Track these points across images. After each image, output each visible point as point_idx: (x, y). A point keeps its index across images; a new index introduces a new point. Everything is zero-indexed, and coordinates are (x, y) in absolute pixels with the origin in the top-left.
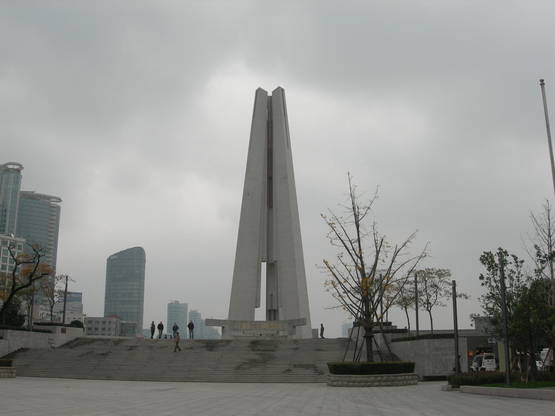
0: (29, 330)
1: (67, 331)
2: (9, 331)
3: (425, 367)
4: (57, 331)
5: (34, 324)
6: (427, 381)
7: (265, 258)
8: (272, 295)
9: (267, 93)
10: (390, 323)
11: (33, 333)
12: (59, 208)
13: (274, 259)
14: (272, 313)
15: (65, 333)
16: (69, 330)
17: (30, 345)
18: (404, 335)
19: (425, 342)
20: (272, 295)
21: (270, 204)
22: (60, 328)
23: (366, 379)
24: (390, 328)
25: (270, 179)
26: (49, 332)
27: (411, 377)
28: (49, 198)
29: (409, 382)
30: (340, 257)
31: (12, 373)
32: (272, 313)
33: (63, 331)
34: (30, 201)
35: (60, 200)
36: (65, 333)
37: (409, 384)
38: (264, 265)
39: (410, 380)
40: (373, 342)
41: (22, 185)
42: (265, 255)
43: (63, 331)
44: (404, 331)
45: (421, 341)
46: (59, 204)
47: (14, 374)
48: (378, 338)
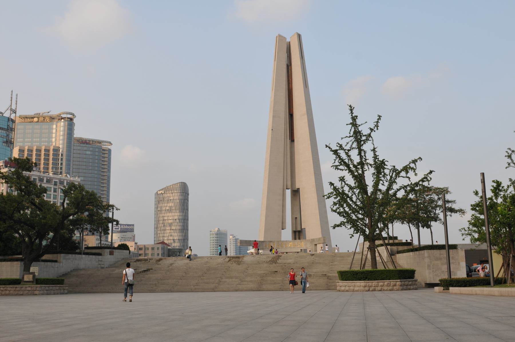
0: (81, 254)
1: (114, 253)
2: (62, 255)
3: (424, 275)
4: (106, 254)
5: (85, 248)
6: (429, 287)
7: (289, 186)
8: (296, 218)
9: (285, 38)
10: (396, 238)
11: (84, 256)
12: (110, 151)
13: (297, 187)
14: (297, 234)
15: (113, 255)
16: (116, 252)
17: (82, 266)
18: (409, 247)
19: (426, 252)
20: (296, 218)
21: (292, 140)
22: (108, 250)
23: (346, 284)
24: (396, 241)
25: (291, 116)
26: (100, 254)
27: (410, 283)
28: (100, 142)
29: (409, 287)
30: (342, 179)
31: (64, 290)
32: (297, 234)
33: (111, 253)
34: (84, 145)
35: (110, 143)
36: (113, 255)
37: (410, 289)
38: (288, 193)
39: (410, 285)
40: (377, 252)
41: (75, 132)
42: (289, 183)
43: (111, 253)
44: (407, 244)
45: (422, 252)
46: (109, 147)
47: (66, 291)
48: (383, 251)
